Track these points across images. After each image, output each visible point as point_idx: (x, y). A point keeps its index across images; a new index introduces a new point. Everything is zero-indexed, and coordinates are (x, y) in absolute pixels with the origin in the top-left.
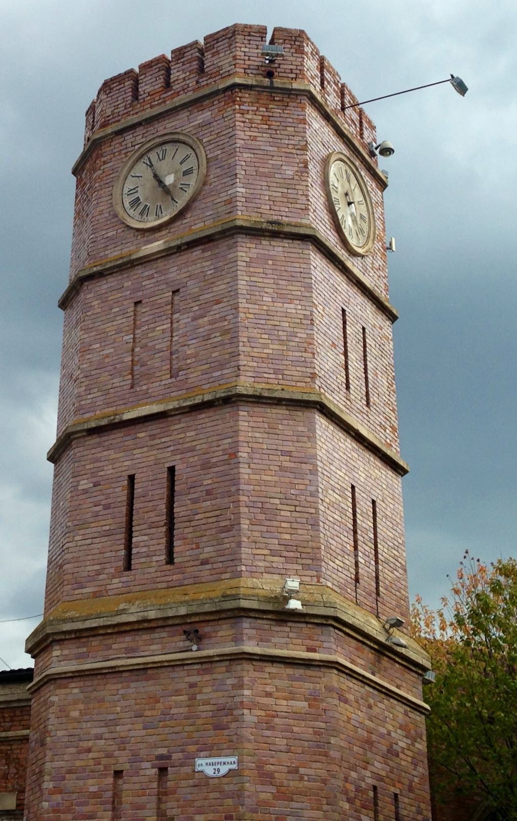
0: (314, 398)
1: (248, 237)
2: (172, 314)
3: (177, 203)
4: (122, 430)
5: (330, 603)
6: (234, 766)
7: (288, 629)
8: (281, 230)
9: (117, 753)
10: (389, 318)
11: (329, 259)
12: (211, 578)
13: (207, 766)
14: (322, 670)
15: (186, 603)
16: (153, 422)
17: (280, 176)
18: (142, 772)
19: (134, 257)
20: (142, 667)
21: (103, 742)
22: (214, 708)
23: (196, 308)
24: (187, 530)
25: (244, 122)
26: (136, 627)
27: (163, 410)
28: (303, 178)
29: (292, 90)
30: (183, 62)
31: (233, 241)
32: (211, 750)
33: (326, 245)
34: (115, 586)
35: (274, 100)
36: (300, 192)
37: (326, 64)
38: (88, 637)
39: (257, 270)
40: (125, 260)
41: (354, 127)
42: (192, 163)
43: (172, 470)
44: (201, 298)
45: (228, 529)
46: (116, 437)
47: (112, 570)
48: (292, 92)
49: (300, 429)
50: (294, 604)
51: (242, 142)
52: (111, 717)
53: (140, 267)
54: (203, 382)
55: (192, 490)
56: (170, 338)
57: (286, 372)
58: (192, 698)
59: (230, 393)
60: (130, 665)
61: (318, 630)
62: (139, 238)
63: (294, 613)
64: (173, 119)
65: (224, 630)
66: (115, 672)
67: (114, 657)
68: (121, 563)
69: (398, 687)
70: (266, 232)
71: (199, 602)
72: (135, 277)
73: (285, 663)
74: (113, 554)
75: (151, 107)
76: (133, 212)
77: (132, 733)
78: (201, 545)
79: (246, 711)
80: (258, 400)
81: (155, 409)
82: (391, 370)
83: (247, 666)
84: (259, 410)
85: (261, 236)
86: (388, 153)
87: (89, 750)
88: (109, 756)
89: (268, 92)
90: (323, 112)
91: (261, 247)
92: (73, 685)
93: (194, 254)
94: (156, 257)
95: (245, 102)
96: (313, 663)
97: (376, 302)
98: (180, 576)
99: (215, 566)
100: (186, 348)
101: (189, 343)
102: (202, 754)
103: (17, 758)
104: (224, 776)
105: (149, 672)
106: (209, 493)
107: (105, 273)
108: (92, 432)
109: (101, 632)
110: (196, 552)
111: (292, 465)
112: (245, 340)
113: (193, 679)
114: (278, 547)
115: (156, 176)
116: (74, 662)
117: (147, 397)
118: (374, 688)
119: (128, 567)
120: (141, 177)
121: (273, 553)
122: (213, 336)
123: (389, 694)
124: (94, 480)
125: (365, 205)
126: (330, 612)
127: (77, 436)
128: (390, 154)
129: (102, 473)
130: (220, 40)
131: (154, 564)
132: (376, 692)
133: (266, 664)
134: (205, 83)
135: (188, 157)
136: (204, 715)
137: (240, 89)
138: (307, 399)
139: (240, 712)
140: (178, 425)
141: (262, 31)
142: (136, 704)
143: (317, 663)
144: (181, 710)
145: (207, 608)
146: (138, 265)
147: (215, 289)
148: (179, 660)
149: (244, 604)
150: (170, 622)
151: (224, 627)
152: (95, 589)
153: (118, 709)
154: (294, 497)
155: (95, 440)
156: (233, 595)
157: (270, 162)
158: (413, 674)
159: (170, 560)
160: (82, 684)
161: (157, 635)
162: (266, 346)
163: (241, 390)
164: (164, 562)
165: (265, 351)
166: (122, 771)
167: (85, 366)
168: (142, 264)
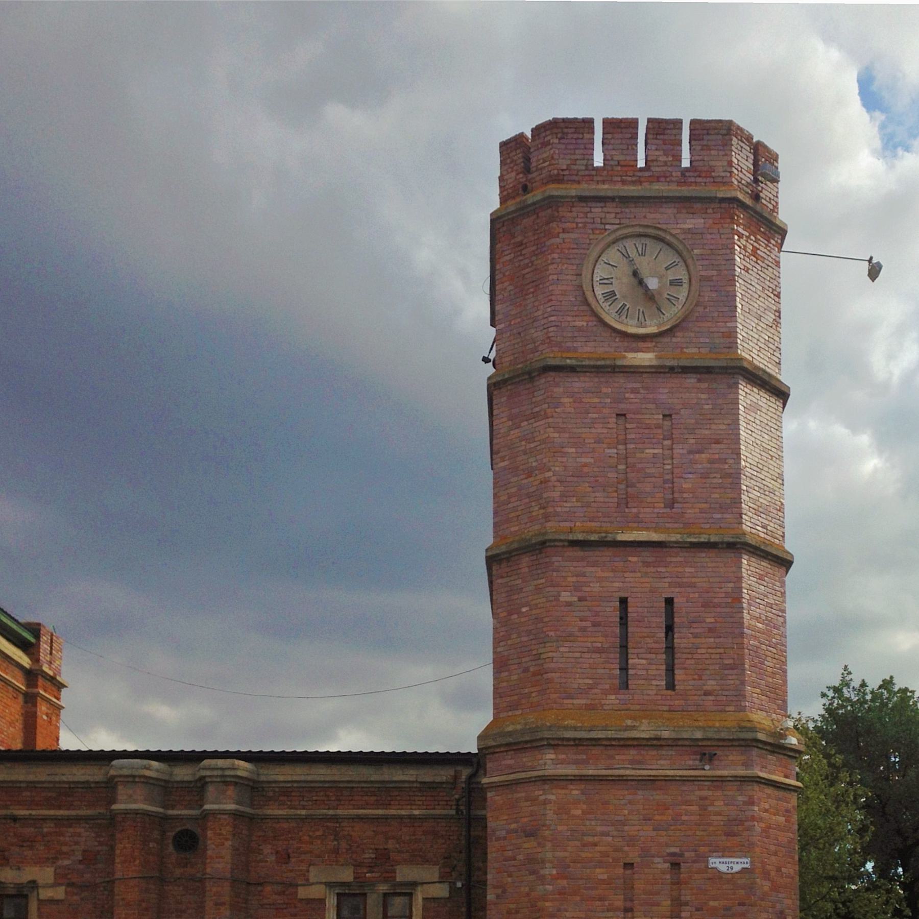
3: (664, 314)
4: (610, 549)
9: (626, 848)
12: (715, 708)
13: (719, 864)
15: (703, 728)
16: (646, 549)
21: (610, 839)
22: (726, 818)
23: (693, 441)
24: (688, 662)
27: (664, 540)
31: (733, 381)
32: (725, 852)
34: (610, 702)
38: (587, 745)
40: (608, 362)
42: (681, 273)
43: (669, 602)
45: (732, 667)
46: (606, 554)
47: (607, 687)
52: (619, 818)
53: (622, 374)
54: (702, 521)
55: (694, 625)
58: (703, 808)
59: (738, 540)
60: (639, 776)
62: (617, 340)
65: (734, 756)
67: (618, 766)
68: (617, 682)
71: (716, 730)
72: (616, 385)
73: (774, 786)
75: (624, 182)
76: (608, 308)
77: (641, 833)
78: (704, 678)
79: (756, 823)
81: (655, 537)
83: (756, 787)
87: (595, 845)
88: (617, 850)
98: (682, 702)
99: (719, 698)
100: (682, 480)
101: (686, 476)
102: (715, 854)
103: (348, 835)
104: (737, 873)
106: (711, 630)
108: (574, 543)
113: (705, 793)
115: (635, 274)
116: (574, 767)
117: (639, 523)
119: (625, 685)
120: (616, 267)
124: (579, 594)
131: (654, 687)
134: (693, 180)
136: (715, 823)
137: (738, 206)
139: (751, 823)
142: (644, 809)
144: (692, 818)
145: (724, 735)
146: (621, 372)
147: (713, 427)
148: (691, 776)
150: (680, 743)
151: (734, 753)
152: (589, 702)
153: (626, 812)
155: (578, 553)
159: (671, 686)
161: (664, 752)
166: (633, 864)
167: (557, 469)
168: (623, 372)
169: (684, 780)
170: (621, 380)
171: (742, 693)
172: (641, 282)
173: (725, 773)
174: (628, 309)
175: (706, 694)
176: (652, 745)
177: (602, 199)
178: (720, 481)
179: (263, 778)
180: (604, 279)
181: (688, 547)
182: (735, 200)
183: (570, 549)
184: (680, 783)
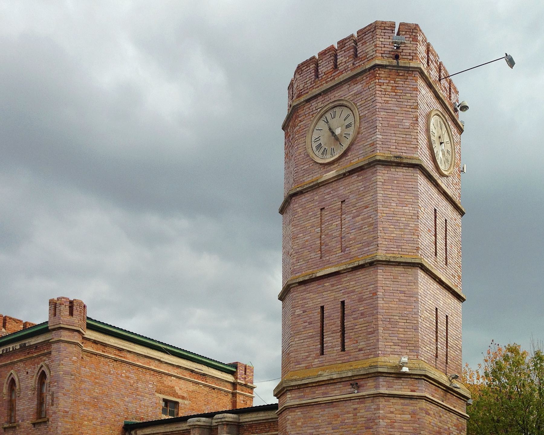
5: (423, 368)
7: (402, 381)
8: (402, 161)
10: (460, 214)
12: (364, 357)
16: (332, 277)
19: (319, 181)
20: (330, 401)
29: (410, 67)
33: (426, 170)
36: (413, 137)
38: (304, 388)
40: (315, 183)
43: (343, 303)
46: (313, 286)
47: (314, 355)
50: (405, 369)
51: (380, 105)
53: (323, 187)
55: (354, 313)
57: (403, 247)
58: (355, 415)
59: (373, 260)
61: (416, 381)
63: (405, 374)
65: (371, 383)
68: (319, 352)
69: (454, 407)
70: (394, 163)
72: (320, 193)
79: (381, 420)
80: (388, 263)
83: (382, 399)
84: (388, 268)
85: (390, 165)
86: (465, 109)
91: (390, 172)
99: (366, 351)
105: (334, 403)
106: (362, 314)
107: (304, 192)
109: (310, 385)
113: (355, 406)
114: (397, 341)
115: (330, 129)
117: (329, 263)
119: (322, 353)
122: (364, 227)
123: (450, 410)
126: (423, 373)
130: (367, 33)
132: (444, 410)
133: (391, 398)
135: (348, 116)
136: (361, 423)
142: (328, 419)
143: (415, 397)
144: (350, 421)
145: (362, 372)
146: (322, 186)
147: (365, 199)
149: (380, 370)
150: (344, 380)
153: (320, 421)
154: (406, 315)
155: (302, 288)
159: (343, 349)
161: (337, 386)
162: (392, 232)
168: (324, 185)
169: (345, 400)
170: (322, 189)
171: (377, 346)
172: (333, 133)
173: (364, 393)
174: (333, 149)
175: (360, 350)
176: (331, 383)
177: (316, 97)
178: (367, 229)
179: (241, 421)
180: (317, 138)
181: (351, 271)
182: (376, 66)
183: (300, 287)
184: (344, 402)
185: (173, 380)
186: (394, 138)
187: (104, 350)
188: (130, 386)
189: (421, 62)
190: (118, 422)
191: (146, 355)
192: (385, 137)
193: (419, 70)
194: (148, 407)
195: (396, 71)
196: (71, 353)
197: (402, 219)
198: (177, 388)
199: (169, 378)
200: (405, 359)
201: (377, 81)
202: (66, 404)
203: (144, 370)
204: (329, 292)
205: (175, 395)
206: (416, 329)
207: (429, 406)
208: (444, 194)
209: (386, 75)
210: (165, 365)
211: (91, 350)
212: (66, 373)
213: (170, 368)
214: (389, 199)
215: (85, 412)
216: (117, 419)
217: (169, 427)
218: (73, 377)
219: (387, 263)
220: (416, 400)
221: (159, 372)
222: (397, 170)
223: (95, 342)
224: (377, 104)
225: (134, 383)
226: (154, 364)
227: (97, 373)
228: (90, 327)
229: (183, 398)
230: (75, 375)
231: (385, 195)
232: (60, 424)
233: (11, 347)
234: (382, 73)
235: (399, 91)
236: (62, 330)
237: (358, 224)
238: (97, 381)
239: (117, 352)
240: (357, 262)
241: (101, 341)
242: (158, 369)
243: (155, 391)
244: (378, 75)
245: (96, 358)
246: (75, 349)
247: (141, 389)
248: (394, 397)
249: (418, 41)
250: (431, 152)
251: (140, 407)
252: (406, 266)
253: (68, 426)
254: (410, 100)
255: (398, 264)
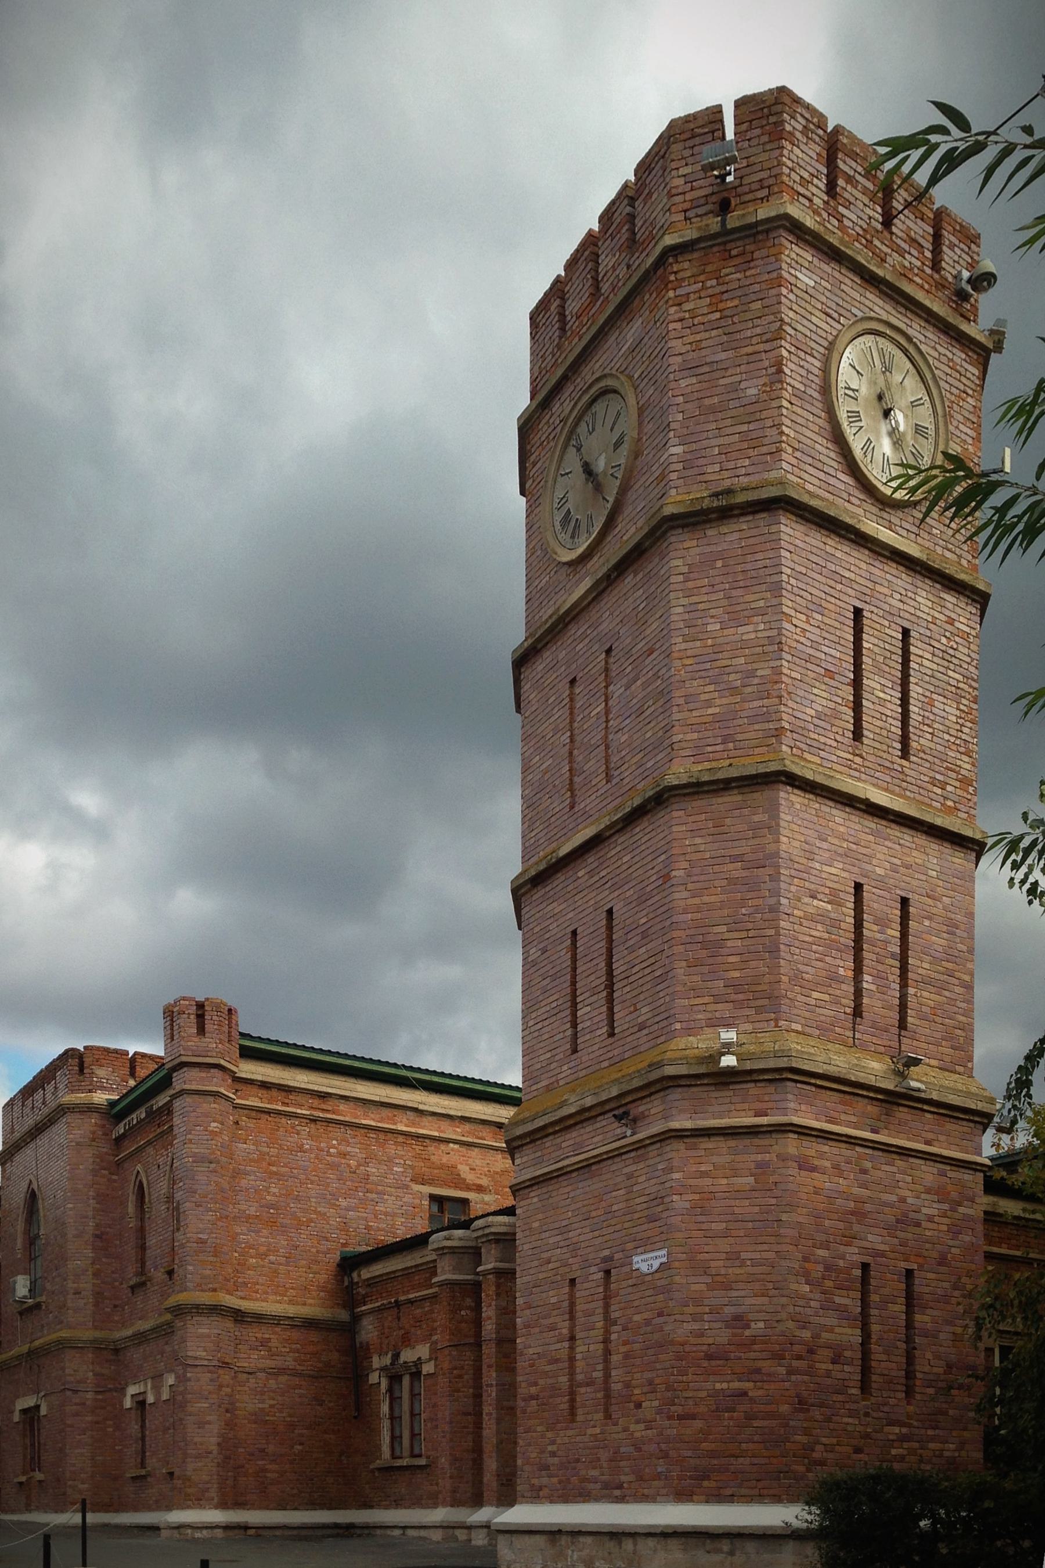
0: (773, 767)
1: (685, 530)
2: (606, 687)
5: (783, 1051)
6: (664, 1260)
7: (731, 1093)
8: (732, 501)
10: (973, 600)
11: (827, 529)
14: (774, 1136)
17: (736, 403)
18: (591, 1278)
19: (562, 611)
20: (585, 1164)
25: (681, 320)
26: (578, 1118)
28: (773, 395)
29: (758, 223)
30: (611, 235)
32: (646, 1245)
33: (811, 507)
35: (731, 257)
36: (769, 423)
37: (845, 141)
39: (699, 583)
41: (915, 252)
43: (610, 912)
44: (634, 650)
48: (760, 228)
49: (756, 818)
50: (728, 1061)
51: (679, 359)
56: (604, 725)
57: (739, 737)
59: (658, 789)
61: (771, 1089)
63: (730, 1072)
64: (600, 353)
65: (654, 1106)
66: (561, 1174)
69: (928, 1143)
70: (713, 512)
74: (561, 1035)
79: (675, 1198)
80: (696, 789)
82: (971, 686)
84: (699, 803)
85: (705, 522)
86: (985, 283)
89: (719, 244)
90: (825, 249)
91: (705, 541)
92: (532, 1194)
93: (626, 581)
94: (586, 602)
95: (683, 279)
96: (762, 1129)
97: (939, 579)
99: (652, 1029)
102: (639, 1250)
104: (656, 1271)
105: (594, 1168)
107: (539, 646)
109: (551, 1130)
110: (634, 1015)
111: (745, 873)
112: (681, 701)
114: (724, 991)
116: (532, 1169)
118: (873, 1148)
121: (717, 999)
123: (905, 1153)
125: (928, 404)
126: (782, 1063)
127: (523, 891)
128: (990, 285)
129: (547, 936)
130: (653, 165)
132: (880, 1153)
133: (701, 1139)
137: (676, 256)
138: (763, 771)
140: (617, 849)
141: (715, 114)
143: (765, 1129)
145: (636, 1083)
147: (648, 632)
149: (670, 1071)
154: (746, 918)
155: (539, 893)
156: (659, 1062)
157: (722, 382)
158: (965, 1123)
160: (539, 1192)
161: (598, 1125)
162: (709, 703)
163: (672, 780)
164: (606, 1035)
165: (710, 711)
168: (573, 619)
175: (642, 1027)
185: (453, 1150)
186: (714, 442)
187: (286, 1101)
188: (349, 1174)
189: (799, 194)
190: (325, 1253)
191: (383, 1100)
192: (694, 446)
193: (784, 222)
194: (394, 1215)
195: (722, 248)
196: (206, 1115)
197: (735, 662)
198: (464, 1170)
199: (443, 1147)
200: (729, 1035)
201: (671, 294)
202: (201, 1226)
203: (382, 1136)
204: (585, 892)
205: (459, 1183)
206: (774, 951)
207: (812, 1148)
208: (897, 559)
209: (695, 270)
210: (430, 1118)
211: (255, 1104)
212: (199, 1159)
213: (445, 1124)
214: (701, 614)
215: (250, 1238)
216: (322, 1248)
217: (409, 1257)
218: (213, 1165)
219: (695, 790)
220: (768, 1136)
221: (418, 1137)
222: (724, 529)
223: (265, 1085)
224: (672, 360)
225: (359, 1165)
226: (405, 1120)
227: (273, 1151)
228: (247, 1054)
229: (480, 1189)
230: (218, 1162)
231: (693, 608)
232: (190, 1268)
233: (134, 1118)
234: (685, 266)
235: (730, 304)
236: (185, 1069)
237: (635, 701)
238: (274, 1169)
239: (316, 1102)
240: (629, 803)
241: (277, 1082)
242: (413, 1130)
243: (408, 1179)
244: (672, 278)
245: (270, 1119)
246: (215, 1106)
247: (375, 1178)
248: (709, 1136)
249: (785, 135)
250: (842, 449)
251: (376, 1217)
252: (749, 785)
253: (208, 1272)
254: (760, 317)
255: (725, 785)
